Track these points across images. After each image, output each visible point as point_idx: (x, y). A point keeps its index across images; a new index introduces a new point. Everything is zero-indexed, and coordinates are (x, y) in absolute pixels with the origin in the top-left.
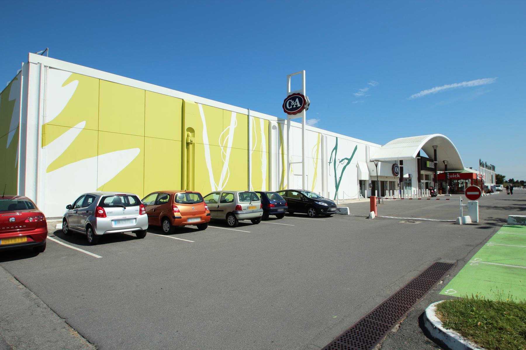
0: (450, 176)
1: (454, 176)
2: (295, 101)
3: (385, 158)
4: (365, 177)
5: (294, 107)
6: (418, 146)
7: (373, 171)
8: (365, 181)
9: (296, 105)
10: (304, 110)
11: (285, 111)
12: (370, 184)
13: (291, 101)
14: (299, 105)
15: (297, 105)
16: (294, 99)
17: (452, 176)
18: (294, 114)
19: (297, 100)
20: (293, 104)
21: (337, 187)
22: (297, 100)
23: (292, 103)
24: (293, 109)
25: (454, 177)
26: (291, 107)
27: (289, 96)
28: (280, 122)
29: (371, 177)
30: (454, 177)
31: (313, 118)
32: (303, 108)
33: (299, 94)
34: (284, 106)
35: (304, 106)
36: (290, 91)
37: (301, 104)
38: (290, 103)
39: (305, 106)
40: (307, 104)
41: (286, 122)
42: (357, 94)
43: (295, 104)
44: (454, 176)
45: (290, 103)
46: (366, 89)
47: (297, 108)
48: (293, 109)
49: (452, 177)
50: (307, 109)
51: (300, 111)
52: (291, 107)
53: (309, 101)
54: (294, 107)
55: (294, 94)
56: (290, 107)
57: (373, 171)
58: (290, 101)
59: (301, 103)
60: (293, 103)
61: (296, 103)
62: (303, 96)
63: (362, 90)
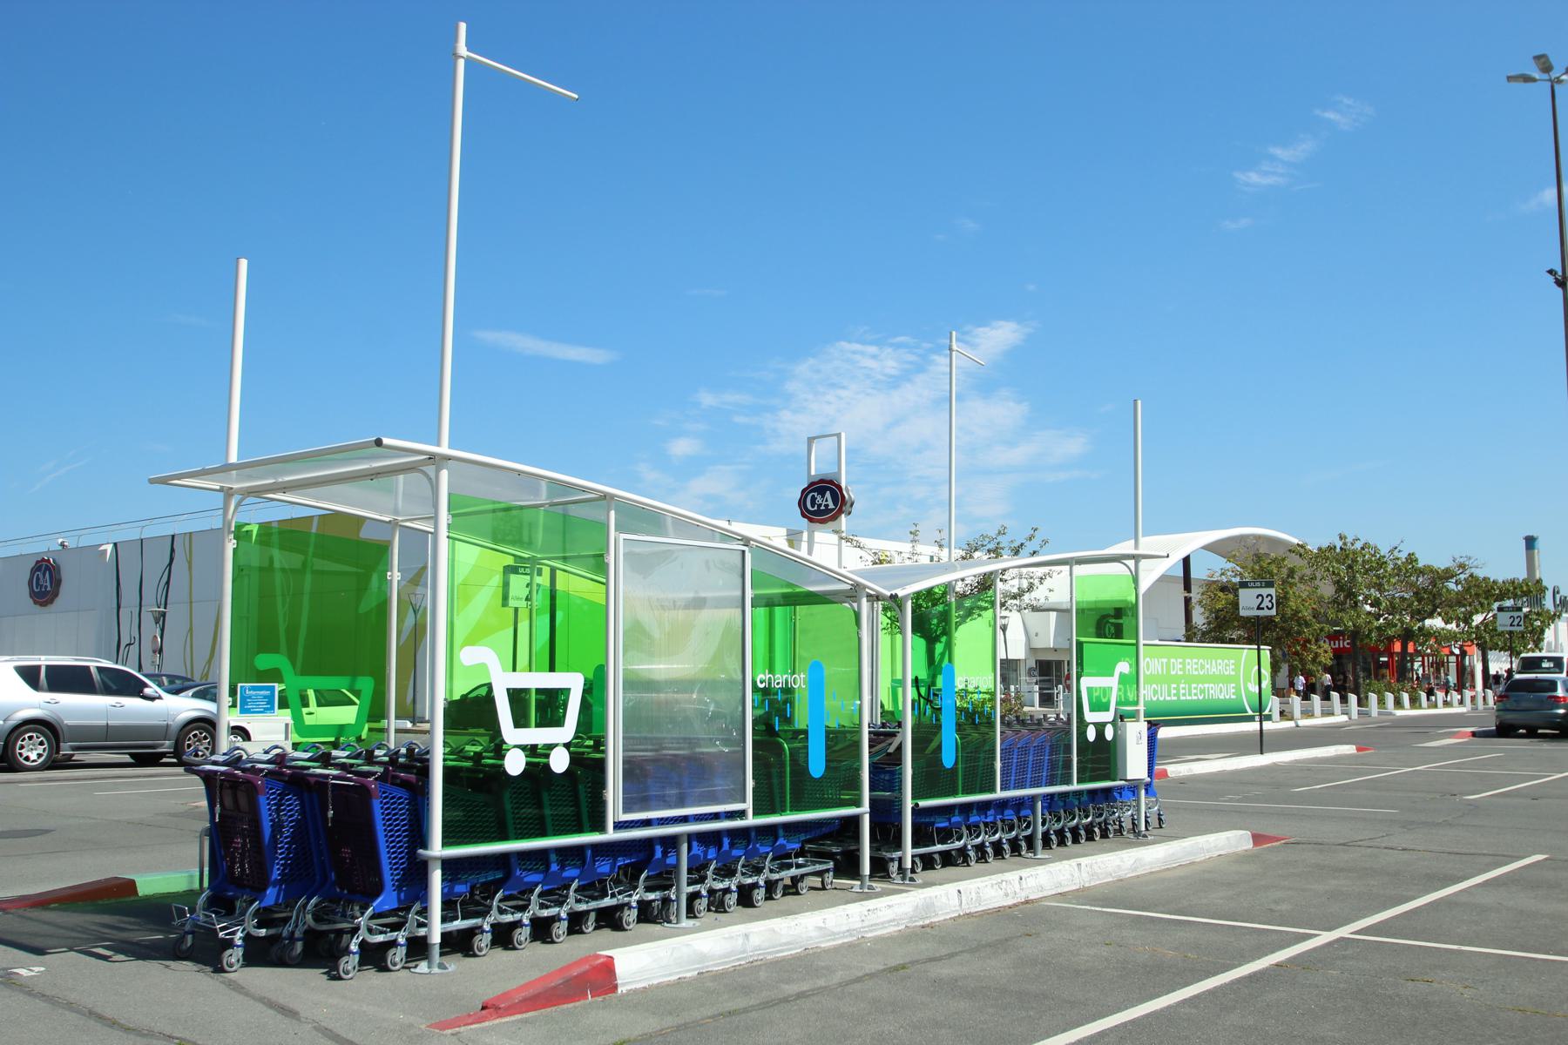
0: (1332, 642)
1: (1341, 642)
2: (823, 497)
3: (1096, 602)
4: (1017, 651)
5: (823, 508)
6: (1152, 570)
7: (1037, 635)
8: (1017, 661)
9: (826, 506)
10: (843, 515)
11: (803, 515)
12: (1030, 669)
13: (816, 494)
14: (831, 506)
15: (828, 505)
17: (1337, 642)
18: (823, 522)
19: (828, 494)
20: (820, 502)
22: (828, 494)
23: (818, 499)
24: (819, 512)
25: (1341, 646)
26: (816, 508)
27: (812, 484)
28: (790, 537)
29: (1032, 650)
30: (1341, 646)
31: (1006, 318)
32: (840, 512)
33: (831, 482)
34: (802, 503)
35: (841, 507)
36: (813, 473)
37: (835, 503)
38: (813, 499)
39: (844, 508)
40: (848, 505)
41: (805, 536)
42: (1254, 177)
43: (824, 503)
44: (1341, 642)
45: (813, 499)
46: (1302, 148)
47: (828, 510)
48: (819, 512)
49: (1337, 646)
50: (850, 513)
51: (835, 518)
52: (816, 508)
53: (852, 496)
54: (823, 508)
55: (821, 481)
56: (813, 507)
57: (1037, 635)
58: (814, 495)
59: (835, 502)
60: (819, 499)
61: (827, 501)
62: (840, 488)
63: (1278, 152)
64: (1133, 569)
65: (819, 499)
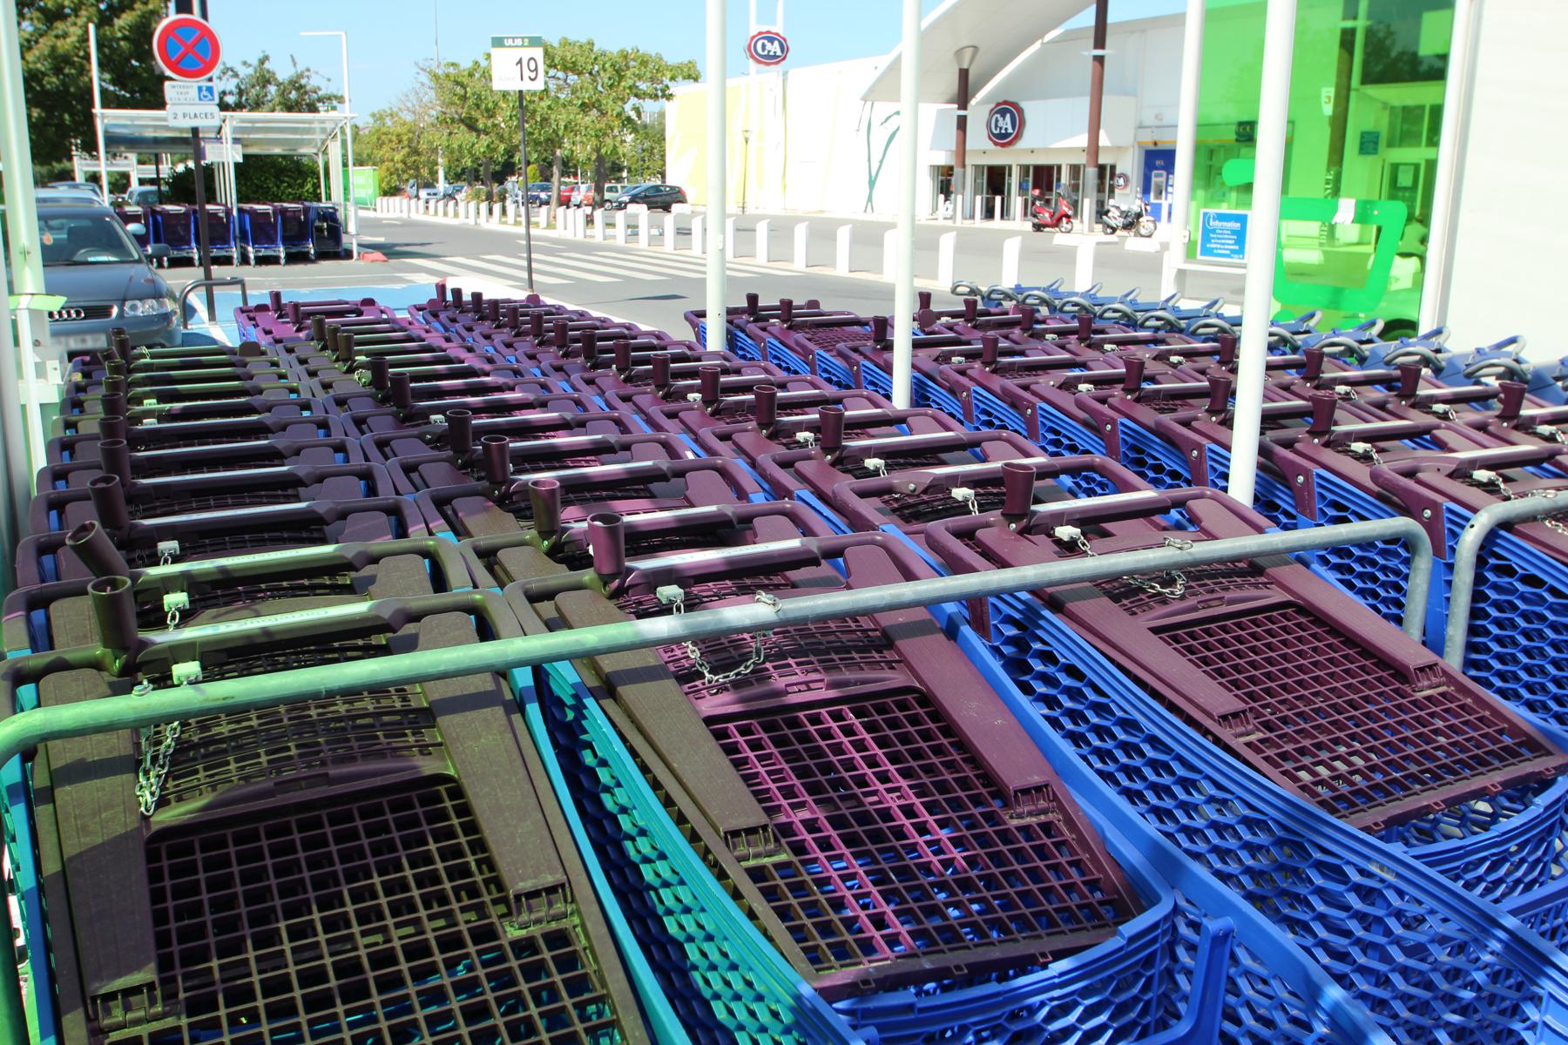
14: (1010, 131)
16: (1003, 113)
19: (776, 43)
21: (872, 183)
22: (776, 43)
24: (768, 57)
38: (997, 121)
45: (997, 121)
60: (769, 46)
64: (874, 174)
65: (1001, 123)
